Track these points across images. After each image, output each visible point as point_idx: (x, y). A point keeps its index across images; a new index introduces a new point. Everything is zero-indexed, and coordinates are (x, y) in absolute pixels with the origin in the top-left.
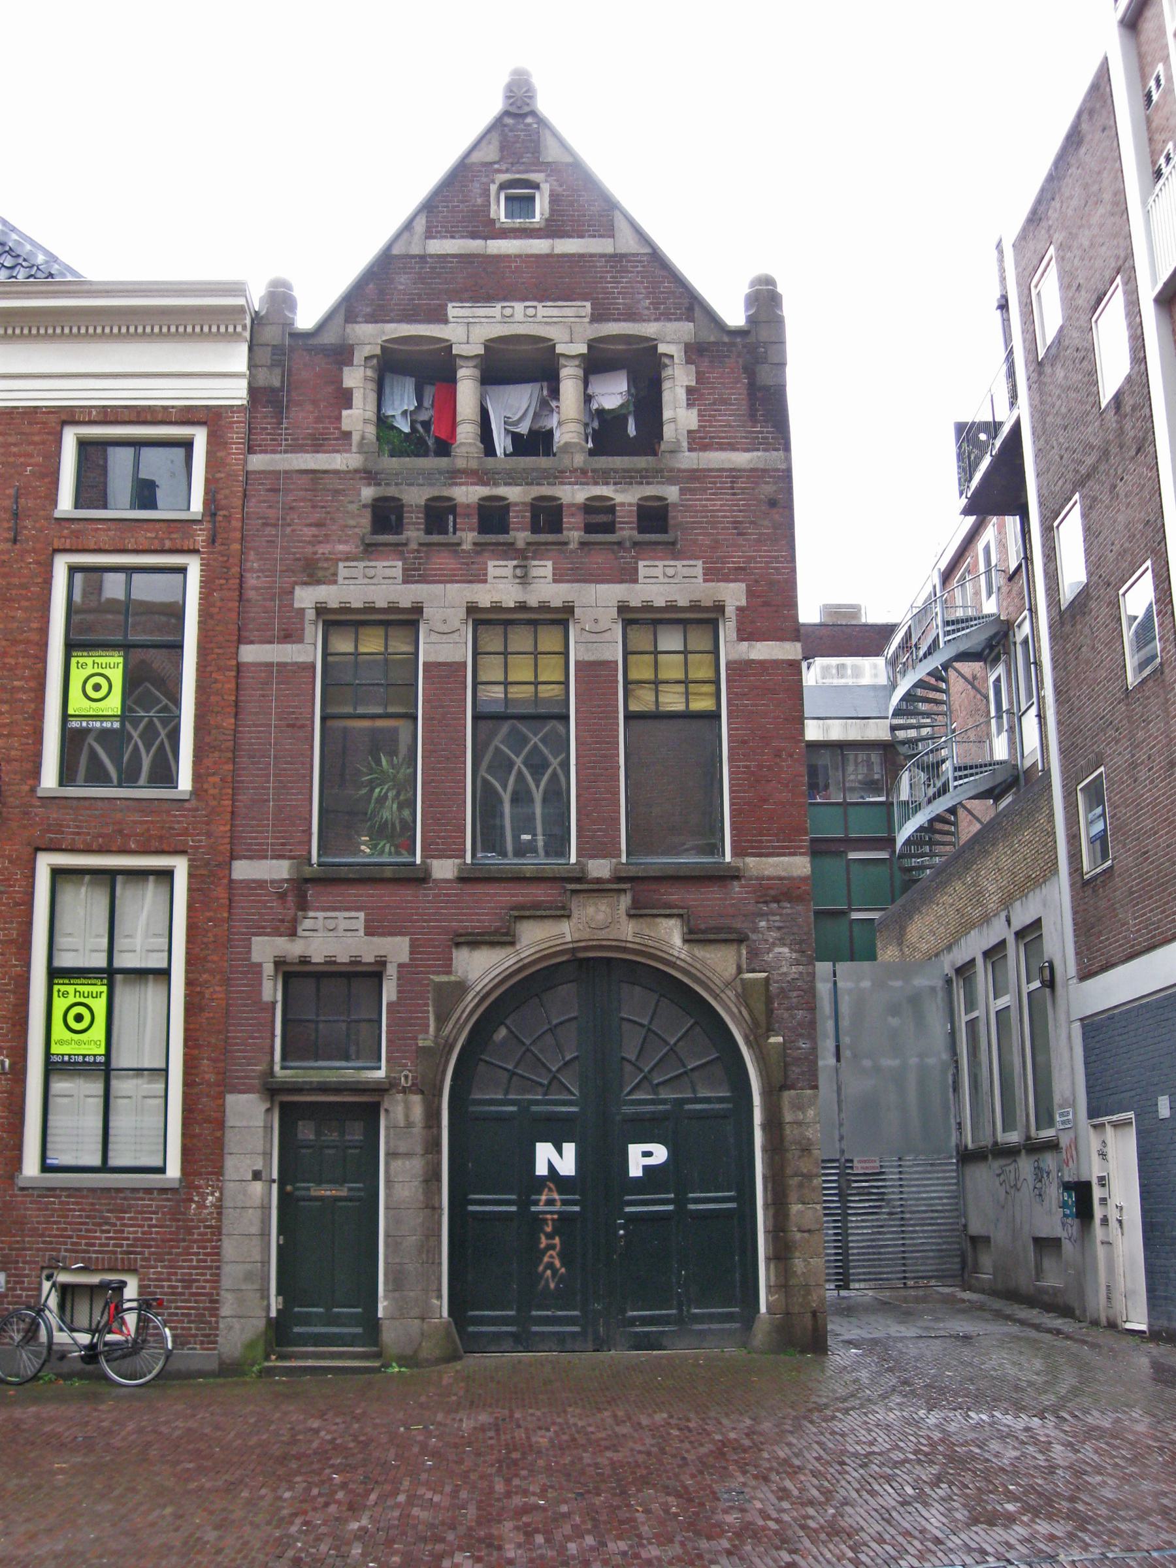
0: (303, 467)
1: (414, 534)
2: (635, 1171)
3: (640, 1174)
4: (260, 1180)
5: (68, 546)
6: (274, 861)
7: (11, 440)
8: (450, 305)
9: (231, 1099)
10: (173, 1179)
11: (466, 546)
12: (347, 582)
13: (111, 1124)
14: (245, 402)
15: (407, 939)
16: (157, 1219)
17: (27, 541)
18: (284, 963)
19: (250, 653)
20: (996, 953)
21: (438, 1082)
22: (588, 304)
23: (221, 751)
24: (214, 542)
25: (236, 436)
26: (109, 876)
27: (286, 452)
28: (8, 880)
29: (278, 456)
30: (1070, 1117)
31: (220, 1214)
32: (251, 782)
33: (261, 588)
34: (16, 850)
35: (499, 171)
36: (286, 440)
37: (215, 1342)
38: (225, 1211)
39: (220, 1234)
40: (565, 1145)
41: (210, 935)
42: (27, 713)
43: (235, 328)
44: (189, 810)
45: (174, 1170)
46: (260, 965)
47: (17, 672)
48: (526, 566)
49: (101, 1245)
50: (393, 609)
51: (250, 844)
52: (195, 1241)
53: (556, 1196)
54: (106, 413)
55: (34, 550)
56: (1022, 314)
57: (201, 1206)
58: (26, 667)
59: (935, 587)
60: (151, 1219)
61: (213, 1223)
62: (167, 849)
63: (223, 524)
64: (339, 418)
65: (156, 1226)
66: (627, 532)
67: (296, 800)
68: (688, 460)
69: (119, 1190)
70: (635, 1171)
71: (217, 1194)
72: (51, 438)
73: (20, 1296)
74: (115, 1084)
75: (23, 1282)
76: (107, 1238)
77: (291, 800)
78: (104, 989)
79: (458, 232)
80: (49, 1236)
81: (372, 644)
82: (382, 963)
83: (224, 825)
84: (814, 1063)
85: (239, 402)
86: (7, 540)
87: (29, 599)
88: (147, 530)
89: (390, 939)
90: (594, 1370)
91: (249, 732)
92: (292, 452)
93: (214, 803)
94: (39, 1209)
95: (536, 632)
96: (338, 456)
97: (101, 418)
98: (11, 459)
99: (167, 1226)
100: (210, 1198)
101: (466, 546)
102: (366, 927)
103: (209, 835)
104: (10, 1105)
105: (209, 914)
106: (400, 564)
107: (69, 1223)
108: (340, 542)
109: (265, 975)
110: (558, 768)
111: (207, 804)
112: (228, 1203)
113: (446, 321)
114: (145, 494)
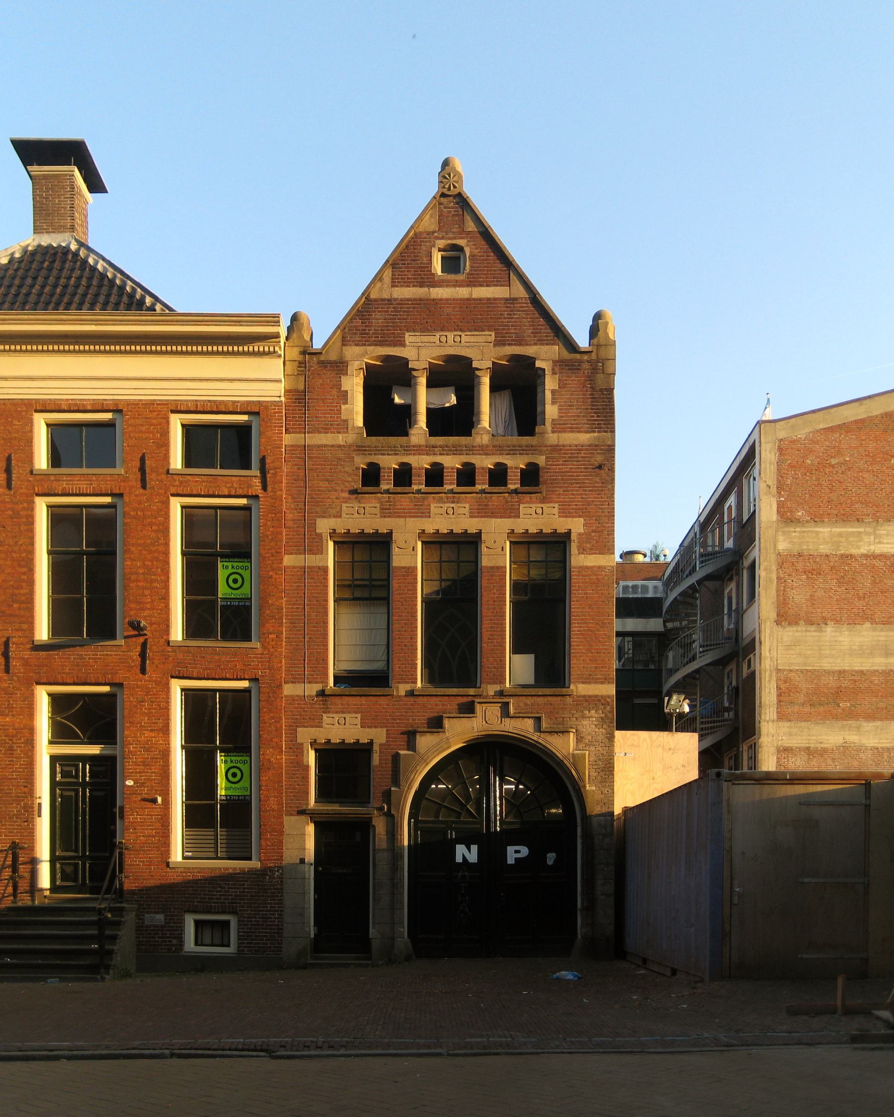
1: (482, 484)
2: (511, 861)
3: (514, 863)
15: (385, 730)
18: (538, 377)
20: (685, 637)
21: (493, 399)
22: (493, 334)
30: (85, 486)
31: (282, 882)
35: (437, 238)
37: (281, 951)
40: (472, 846)
48: (765, 620)
49: (216, 899)
53: (467, 874)
56: (213, 1055)
59: (696, 534)
60: (244, 885)
61: (279, 887)
64: (339, 411)
66: (514, 484)
68: (552, 438)
70: (511, 861)
72: (163, 421)
75: (267, 907)
82: (371, 743)
84: (659, 655)
90: (785, 682)
95: (529, 546)
110: (103, 892)
113: (403, 344)
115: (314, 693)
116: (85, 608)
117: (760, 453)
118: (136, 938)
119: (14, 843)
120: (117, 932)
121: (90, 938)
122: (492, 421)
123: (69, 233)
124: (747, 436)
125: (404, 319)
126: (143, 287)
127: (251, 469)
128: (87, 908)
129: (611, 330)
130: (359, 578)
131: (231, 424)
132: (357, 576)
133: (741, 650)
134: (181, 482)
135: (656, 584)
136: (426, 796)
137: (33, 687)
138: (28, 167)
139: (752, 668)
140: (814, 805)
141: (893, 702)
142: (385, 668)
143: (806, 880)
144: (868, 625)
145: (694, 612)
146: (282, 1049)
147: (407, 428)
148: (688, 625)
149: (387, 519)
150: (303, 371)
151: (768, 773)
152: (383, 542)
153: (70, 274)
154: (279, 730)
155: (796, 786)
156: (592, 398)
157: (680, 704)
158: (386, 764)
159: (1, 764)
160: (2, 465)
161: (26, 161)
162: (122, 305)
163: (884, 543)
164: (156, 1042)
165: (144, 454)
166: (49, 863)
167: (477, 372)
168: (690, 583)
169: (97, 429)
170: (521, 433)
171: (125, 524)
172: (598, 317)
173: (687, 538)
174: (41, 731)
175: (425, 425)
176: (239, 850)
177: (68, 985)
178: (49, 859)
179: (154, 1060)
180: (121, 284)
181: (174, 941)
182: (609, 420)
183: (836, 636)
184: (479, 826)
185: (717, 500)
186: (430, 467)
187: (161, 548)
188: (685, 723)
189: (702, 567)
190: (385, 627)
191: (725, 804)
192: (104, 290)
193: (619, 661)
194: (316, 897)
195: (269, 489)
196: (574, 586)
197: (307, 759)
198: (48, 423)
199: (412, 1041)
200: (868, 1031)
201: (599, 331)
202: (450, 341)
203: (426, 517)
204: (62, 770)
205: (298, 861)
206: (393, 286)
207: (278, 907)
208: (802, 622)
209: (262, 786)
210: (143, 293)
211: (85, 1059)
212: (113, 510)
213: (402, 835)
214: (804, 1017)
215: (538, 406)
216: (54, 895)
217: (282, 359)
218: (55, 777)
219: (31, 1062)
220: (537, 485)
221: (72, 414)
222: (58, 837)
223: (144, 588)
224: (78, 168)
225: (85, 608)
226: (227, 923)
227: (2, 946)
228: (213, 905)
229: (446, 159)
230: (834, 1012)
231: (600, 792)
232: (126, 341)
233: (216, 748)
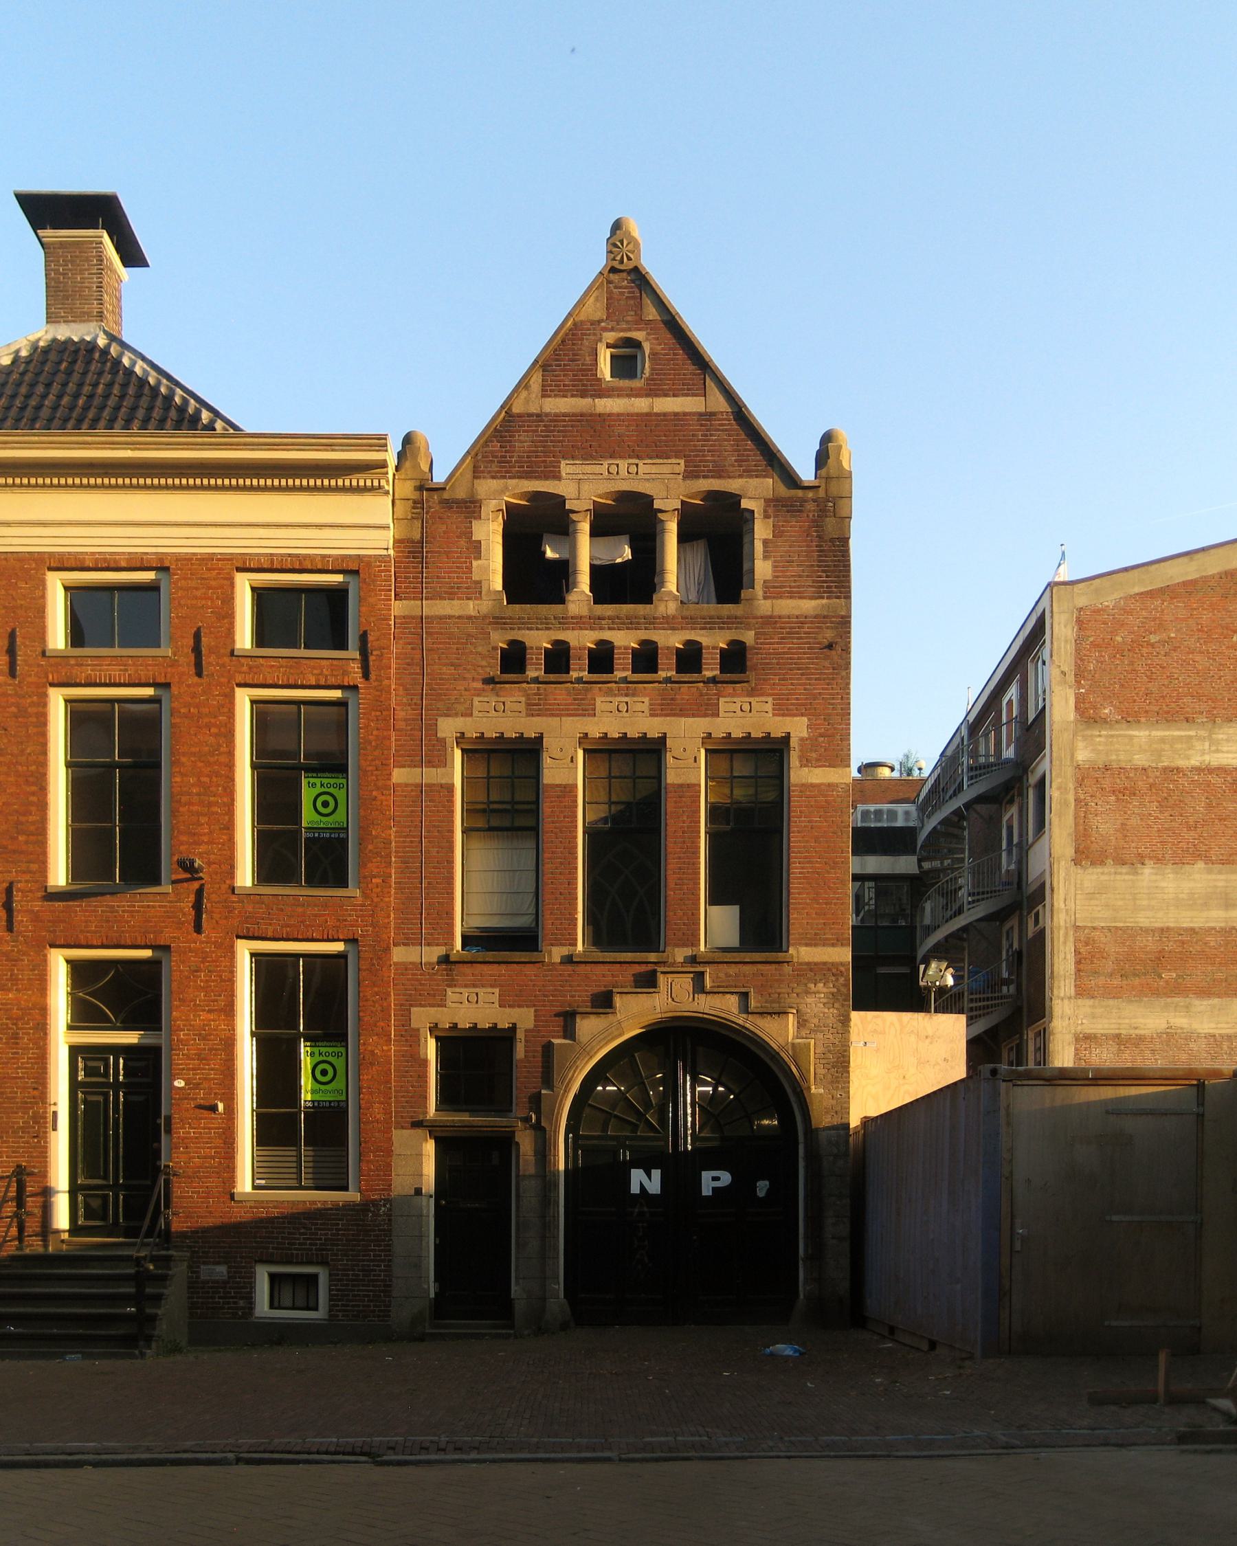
1: (667, 670)
2: (706, 1191)
3: (711, 1194)
15: (532, 1010)
20: (947, 881)
21: (682, 552)
22: (682, 462)
30: (117, 673)
31: (390, 1220)
33: (409, 720)
35: (605, 329)
37: (389, 1316)
40: (653, 1171)
48: (1058, 858)
49: (299, 1244)
56: (294, 1460)
59: (962, 739)
60: (338, 1224)
61: (386, 1227)
64: (470, 569)
66: (711, 670)
68: (764, 606)
70: (706, 1191)
72: (225, 582)
82: (513, 1028)
90: (1087, 944)
95: (732, 756)
110: (142, 1234)
113: (557, 477)
115: (435, 960)
116: (118, 842)
117: (1052, 628)
118: (189, 1298)
119: (19, 1166)
120: (161, 1291)
121: (125, 1299)
122: (680, 583)
123: (95, 323)
124: (1034, 603)
125: (559, 442)
126: (198, 397)
127: (348, 649)
128: (120, 1256)
129: (845, 457)
130: (497, 800)
131: (320, 587)
132: (494, 797)
133: (1025, 900)
134: (250, 668)
135: (907, 809)
136: (590, 1102)
137: (46, 952)
138: (38, 231)
139: (1041, 925)
140: (1126, 1114)
141: (1236, 971)
142: (533, 925)
143: (1115, 1218)
144: (1200, 865)
145: (960, 846)
146: (391, 1452)
147: (563, 592)
148: (953, 865)
149: (535, 719)
150: (419, 514)
151: (1062, 1070)
152: (530, 751)
153: (96, 380)
154: (386, 1011)
155: (1102, 1088)
156: (818, 551)
157: (941, 975)
158: (534, 1057)
159: (1, 1058)
160: (3, 643)
161: (37, 223)
162: (169, 423)
163: (1223, 752)
164: (216, 1442)
165: (199, 629)
166: (67, 1195)
167: (660, 515)
168: (955, 807)
169: (134, 594)
170: (721, 599)
171: (173, 726)
172: (827, 438)
173: (951, 744)
174: (57, 1012)
175: (588, 588)
176: (330, 1176)
177: (94, 1364)
178: (67, 1189)
179: (213, 1468)
180: (167, 393)
181: (241, 1303)
182: (842, 581)
183: (1156, 881)
184: (662, 1143)
185: (991, 692)
186: (594, 647)
187: (223, 759)
188: (947, 1001)
189: (972, 784)
190: (533, 867)
191: (1003, 1112)
192: (144, 402)
193: (857, 915)
194: (438, 1242)
195: (373, 676)
196: (795, 811)
197: (424, 1051)
198: (67, 585)
199: (571, 1440)
200: (1201, 1427)
201: (829, 458)
202: (623, 472)
203: (589, 715)
204: (86, 1066)
205: (412, 1192)
206: (543, 396)
207: (385, 1256)
208: (1110, 861)
209: (363, 1088)
210: (198, 406)
211: (118, 1466)
212: (157, 706)
213: (556, 1155)
214: (1113, 1408)
215: (744, 561)
216: (75, 1239)
217: (390, 497)
218: (77, 1075)
219: (42, 1470)
220: (743, 671)
221: (99, 572)
222: (80, 1158)
223: (199, 814)
224: (107, 232)
225: (118, 842)
226: (315, 1277)
227: (2, 1310)
228: (295, 1252)
229: (617, 220)
230: (1154, 1400)
231: (830, 1096)
232: (174, 471)
233: (299, 1035)
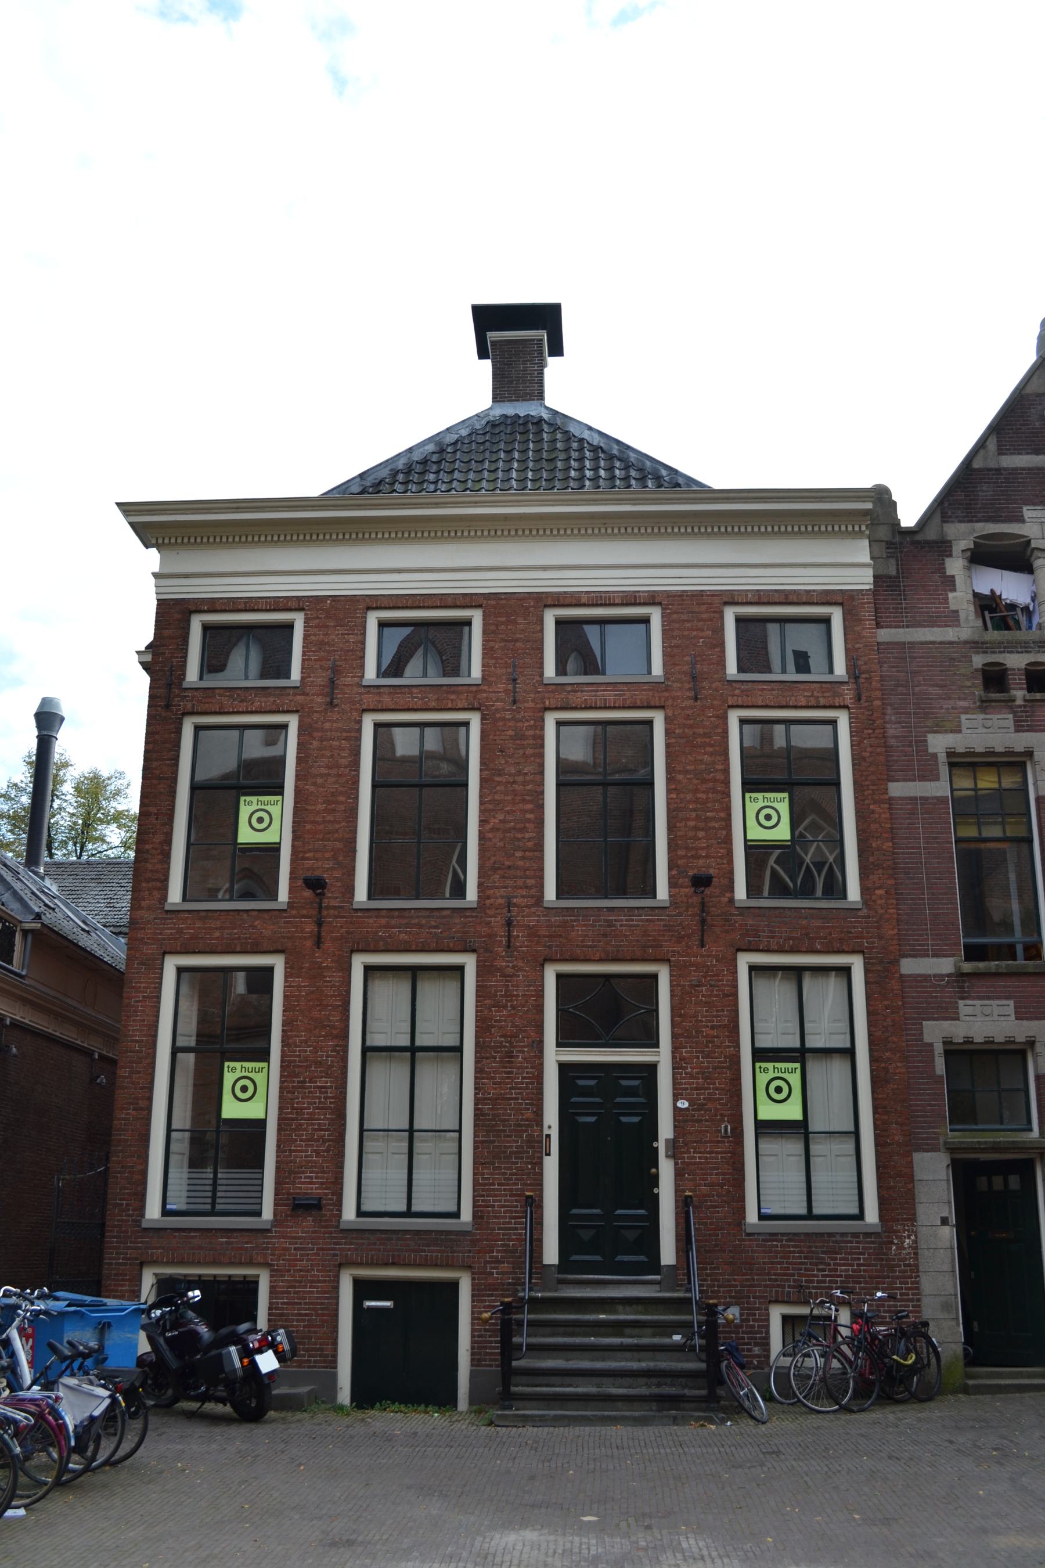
0: (923, 639)
4: (948, 1224)
5: (740, 703)
6: (935, 959)
7: (684, 617)
8: (1025, 508)
9: (917, 1157)
10: (266, 1221)
11: (1019, 702)
12: (969, 731)
13: (414, 1176)
14: (872, 587)
16: (864, 1259)
17: (706, 698)
18: (951, 1043)
19: (897, 789)
23: (883, 868)
24: (859, 699)
25: (867, 614)
26: (797, 972)
27: (907, 627)
28: (718, 975)
29: (901, 630)
31: (916, 1254)
32: (909, 894)
34: (721, 951)
36: (906, 617)
38: (919, 1251)
39: (918, 1271)
41: (889, 1020)
42: (720, 838)
43: (860, 527)
44: (862, 917)
45: (872, 1215)
46: (931, 1045)
47: (709, 805)
49: (818, 1282)
50: (1010, 753)
51: (914, 945)
52: (898, 1278)
54: (759, 595)
55: (712, 707)
57: (901, 1247)
58: (715, 801)
62: (847, 949)
63: (866, 685)
64: (946, 599)
65: (863, 1265)
67: (948, 909)
69: (830, 1235)
71: (913, 1237)
73: (753, 1326)
74: (814, 1148)
76: (823, 1276)
77: (943, 909)
78: (798, 1065)
79: (1024, 449)
80: (775, 1274)
81: (987, 781)
83: (893, 929)
85: (867, 587)
86: (690, 698)
87: (711, 746)
88: (804, 690)
89: (1036, 1022)
91: (903, 853)
92: (912, 626)
93: (881, 911)
94: (765, 1252)
96: (950, 629)
97: (756, 599)
98: (686, 633)
99: (873, 1265)
100: (907, 1241)
101: (1019, 702)
102: (1016, 1012)
103: (880, 937)
104: (734, 1163)
105: (886, 1003)
106: (1011, 716)
107: (791, 1263)
108: (960, 699)
109: (936, 1053)
111: (877, 913)
112: (922, 1245)
113: (1023, 521)
114: (802, 662)
